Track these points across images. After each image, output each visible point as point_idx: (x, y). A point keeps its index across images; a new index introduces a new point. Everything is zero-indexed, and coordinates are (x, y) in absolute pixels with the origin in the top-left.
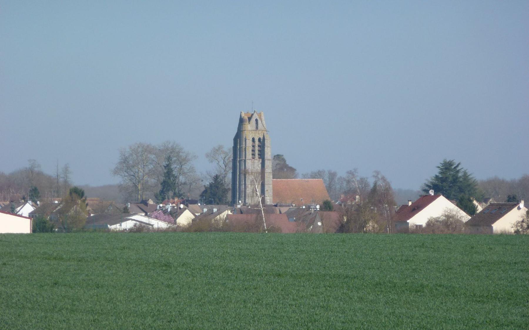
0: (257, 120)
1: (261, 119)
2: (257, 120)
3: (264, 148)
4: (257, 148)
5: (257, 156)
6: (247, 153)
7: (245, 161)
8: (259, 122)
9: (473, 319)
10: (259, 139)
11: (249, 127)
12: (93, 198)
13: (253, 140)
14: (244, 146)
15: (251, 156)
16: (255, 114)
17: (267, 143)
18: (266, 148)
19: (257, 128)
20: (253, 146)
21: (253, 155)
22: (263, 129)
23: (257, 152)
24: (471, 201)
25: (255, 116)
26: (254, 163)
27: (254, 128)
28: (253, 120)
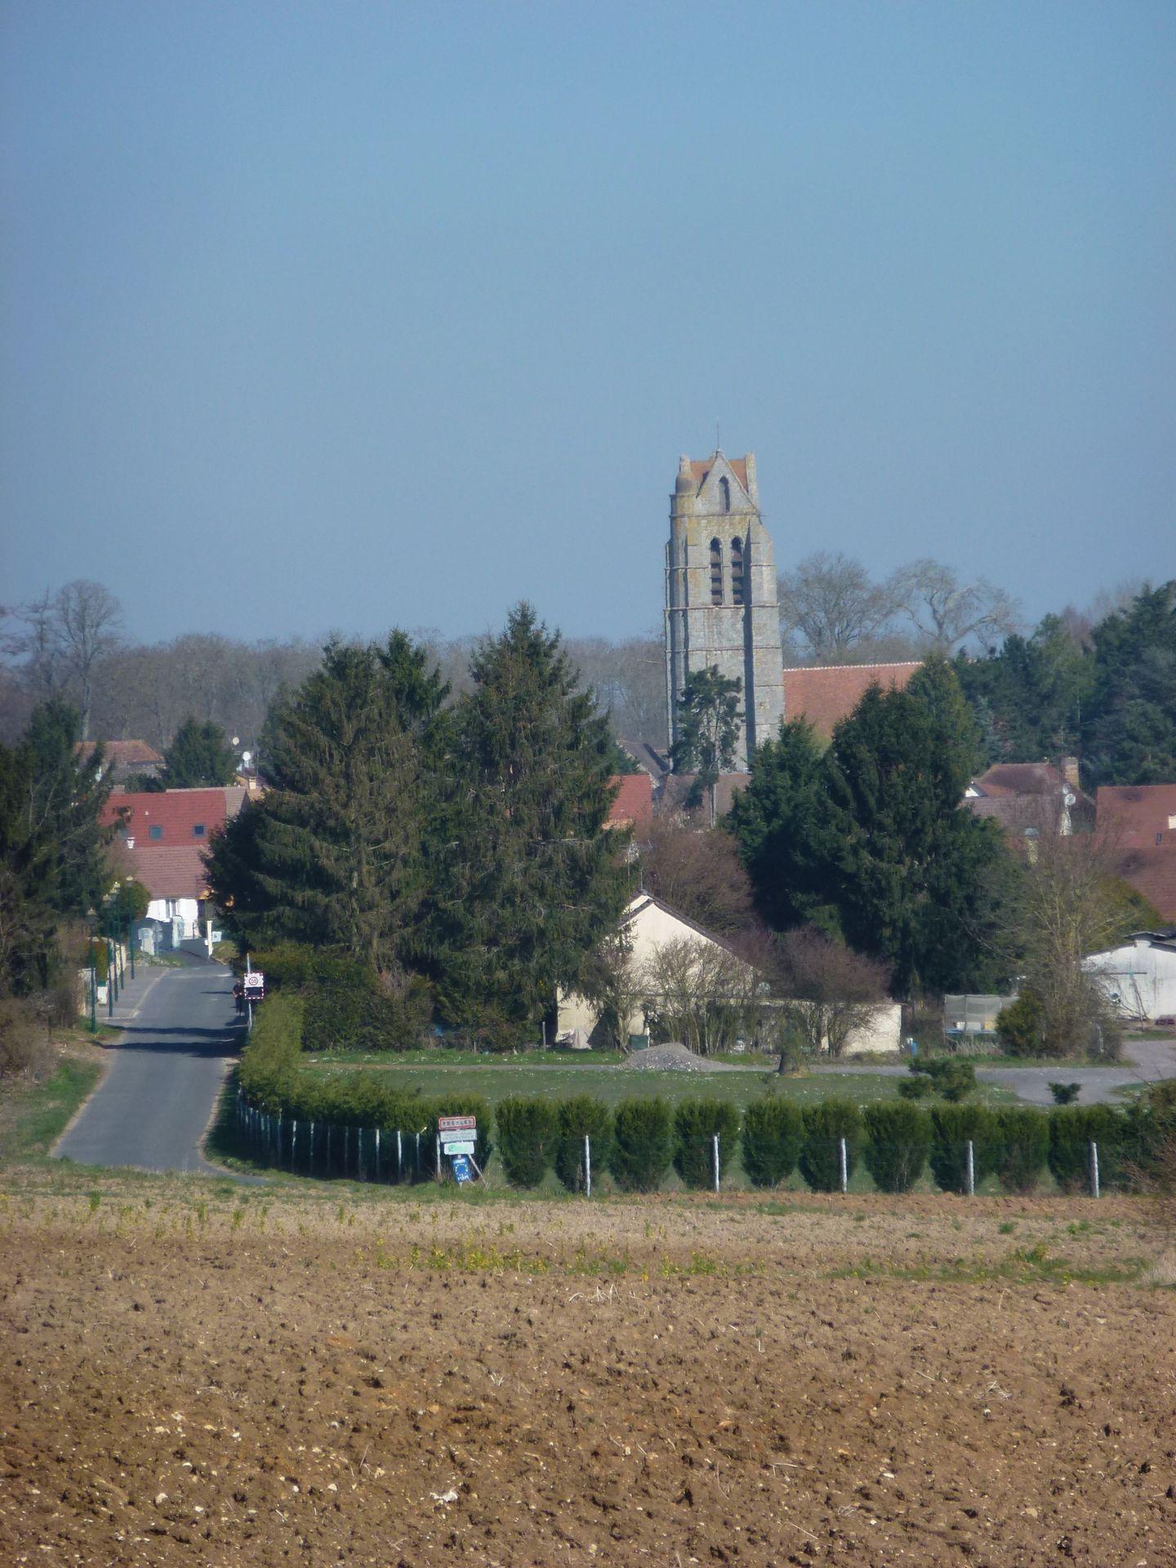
0: (724, 481)
1: (744, 478)
2: (724, 481)
3: (748, 567)
4: (728, 572)
5: (729, 596)
6: (690, 586)
7: (685, 612)
8: (734, 486)
9: (872, 1422)
10: (736, 543)
11: (698, 505)
12: (669, 656)
13: (715, 545)
14: (682, 565)
15: (707, 598)
16: (719, 461)
17: (761, 554)
18: (753, 569)
19: (728, 506)
20: (716, 565)
21: (717, 592)
22: (745, 507)
23: (728, 585)
24: (374, 1128)
25: (720, 469)
26: (719, 619)
27: (717, 508)
28: (714, 481)
